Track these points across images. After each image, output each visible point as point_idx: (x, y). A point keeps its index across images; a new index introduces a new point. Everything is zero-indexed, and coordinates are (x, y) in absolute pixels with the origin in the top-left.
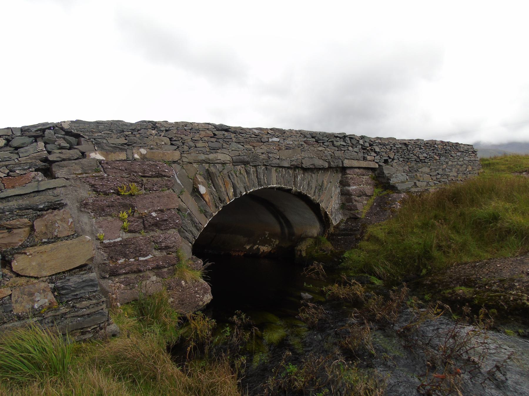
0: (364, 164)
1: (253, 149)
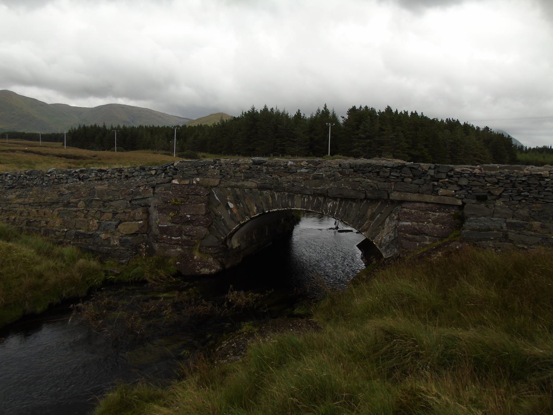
0: (432, 199)
1: (279, 179)
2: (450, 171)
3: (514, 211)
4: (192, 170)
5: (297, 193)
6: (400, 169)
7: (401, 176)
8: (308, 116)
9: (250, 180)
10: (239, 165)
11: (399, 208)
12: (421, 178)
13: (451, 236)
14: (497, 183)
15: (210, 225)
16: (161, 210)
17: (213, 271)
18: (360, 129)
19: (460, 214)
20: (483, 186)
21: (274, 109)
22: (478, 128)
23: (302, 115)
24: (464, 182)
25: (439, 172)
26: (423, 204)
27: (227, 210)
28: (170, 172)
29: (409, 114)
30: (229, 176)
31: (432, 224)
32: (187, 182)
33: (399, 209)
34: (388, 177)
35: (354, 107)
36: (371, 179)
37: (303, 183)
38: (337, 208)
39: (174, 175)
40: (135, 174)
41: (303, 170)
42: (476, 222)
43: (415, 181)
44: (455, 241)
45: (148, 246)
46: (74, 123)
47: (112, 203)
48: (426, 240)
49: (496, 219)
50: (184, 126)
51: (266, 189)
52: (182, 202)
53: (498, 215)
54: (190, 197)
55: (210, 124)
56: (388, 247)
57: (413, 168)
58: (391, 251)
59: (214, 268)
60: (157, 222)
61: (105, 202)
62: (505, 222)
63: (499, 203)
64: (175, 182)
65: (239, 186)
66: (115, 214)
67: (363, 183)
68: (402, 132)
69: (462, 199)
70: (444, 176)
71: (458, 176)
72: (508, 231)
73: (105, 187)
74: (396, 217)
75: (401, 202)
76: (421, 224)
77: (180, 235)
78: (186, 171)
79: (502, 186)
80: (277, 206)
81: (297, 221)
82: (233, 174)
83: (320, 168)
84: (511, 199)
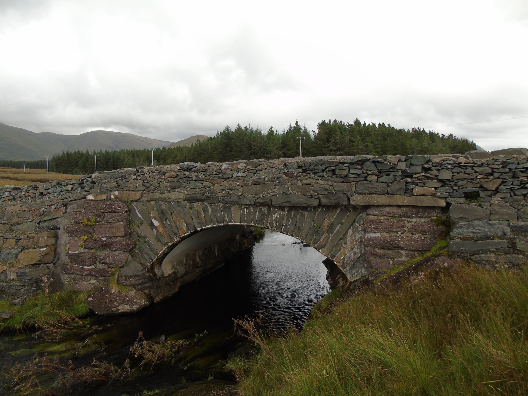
0: (406, 200)
1: (211, 187)
2: (427, 162)
3: (519, 210)
4: (112, 182)
5: (233, 203)
6: (361, 165)
7: (363, 173)
8: (280, 133)
9: (177, 190)
10: (164, 173)
11: (363, 215)
12: (388, 175)
13: (435, 248)
14: (491, 174)
15: (132, 250)
16: (71, 233)
17: (135, 307)
18: (330, 141)
19: (444, 218)
20: (472, 179)
21: (248, 127)
22: (443, 136)
23: (275, 132)
24: (446, 175)
25: (411, 164)
26: (394, 208)
27: (152, 229)
28: (87, 186)
29: (377, 126)
30: (153, 187)
31: (409, 235)
32: (104, 197)
33: (364, 216)
34: (346, 176)
35: (324, 122)
36: (325, 181)
37: (241, 190)
38: (285, 220)
39: (91, 189)
40: (49, 191)
41: (240, 174)
42: (468, 228)
43: (382, 179)
44: (439, 255)
45: (51, 279)
46: (59, 151)
47: (19, 227)
48: (402, 256)
49: (495, 222)
50: (164, 149)
51: (197, 200)
52: (96, 222)
53: (497, 217)
54: (106, 214)
55: (189, 145)
56: (353, 267)
57: (378, 162)
58: (357, 271)
59: (136, 303)
60: (67, 248)
61: (12, 225)
62: (509, 225)
63: (496, 200)
64: (91, 197)
65: (164, 199)
66: (18, 240)
67: (315, 185)
68: (372, 142)
69: (446, 198)
70: (419, 169)
71: (437, 168)
72: (515, 238)
73: (17, 208)
74: (360, 228)
75: (366, 207)
76: (394, 234)
77: (94, 263)
78: (105, 183)
79: (498, 178)
80: (212, 222)
81: (259, 237)
82: (157, 185)
83: (261, 171)
84: (512, 194)
